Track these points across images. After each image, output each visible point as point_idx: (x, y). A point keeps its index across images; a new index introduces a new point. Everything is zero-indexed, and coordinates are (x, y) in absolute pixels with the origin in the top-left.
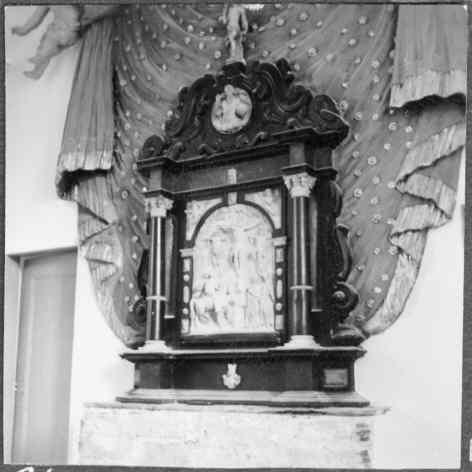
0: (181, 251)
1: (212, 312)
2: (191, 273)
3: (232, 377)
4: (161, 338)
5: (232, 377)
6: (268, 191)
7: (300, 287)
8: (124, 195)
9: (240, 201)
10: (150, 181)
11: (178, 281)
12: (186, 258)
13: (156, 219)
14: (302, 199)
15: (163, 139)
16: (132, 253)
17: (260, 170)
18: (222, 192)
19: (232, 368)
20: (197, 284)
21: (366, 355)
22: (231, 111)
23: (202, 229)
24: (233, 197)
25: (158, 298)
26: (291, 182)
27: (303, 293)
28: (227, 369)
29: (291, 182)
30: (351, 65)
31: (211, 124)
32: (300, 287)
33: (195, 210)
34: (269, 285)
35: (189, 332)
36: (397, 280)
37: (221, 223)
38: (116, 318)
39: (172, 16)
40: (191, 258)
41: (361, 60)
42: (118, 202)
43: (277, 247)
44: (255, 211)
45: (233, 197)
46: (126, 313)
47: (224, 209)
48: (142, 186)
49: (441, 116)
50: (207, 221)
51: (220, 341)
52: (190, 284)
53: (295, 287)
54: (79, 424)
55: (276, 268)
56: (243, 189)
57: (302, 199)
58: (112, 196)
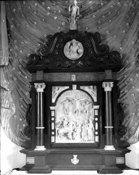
0: (50, 107)
2: (54, 117)
3: (75, 161)
5: (75, 161)
6: (92, 87)
7: (109, 127)
8: (15, 79)
11: (48, 119)
14: (41, 93)
15: (110, 51)
16: (20, 106)
17: (88, 76)
18: (70, 84)
19: (75, 156)
20: (58, 120)
22: (74, 51)
23: (59, 98)
24: (75, 87)
26: (37, 86)
27: (111, 129)
30: (122, 42)
32: (109, 127)
33: (56, 91)
34: (91, 125)
35: (55, 142)
37: (67, 96)
38: (15, 132)
41: (55, 46)
42: (11, 81)
44: (85, 94)
45: (75, 87)
46: (17, 132)
47: (69, 91)
48: (25, 76)
50: (62, 95)
52: (54, 121)
55: (95, 118)
56: (79, 84)
57: (41, 93)
58: (7, 79)
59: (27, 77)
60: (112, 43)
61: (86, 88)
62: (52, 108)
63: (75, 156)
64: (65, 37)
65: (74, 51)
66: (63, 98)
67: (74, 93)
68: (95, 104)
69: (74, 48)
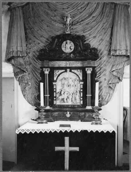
1: (63, 99)
2: (56, 89)
4: (49, 106)
9: (70, 71)
10: (65, 95)
11: (51, 90)
12: (55, 85)
13: (47, 74)
19: (68, 113)
21: (102, 110)
22: (68, 47)
23: (59, 77)
24: (68, 70)
25: (48, 95)
27: (90, 97)
28: (67, 113)
29: (88, 70)
31: (62, 49)
36: (84, 65)
39: (80, 43)
40: (56, 85)
43: (81, 84)
45: (68, 70)
47: (65, 73)
49: (108, 42)
51: (65, 106)
52: (56, 91)
53: (88, 95)
54: (15, 90)
55: (81, 90)
59: (39, 64)
60: (94, 43)
61: (75, 71)
62: (54, 83)
63: (68, 113)
64: (64, 37)
65: (68, 47)
66: (61, 77)
67: (68, 74)
68: (80, 81)
69: (68, 46)
